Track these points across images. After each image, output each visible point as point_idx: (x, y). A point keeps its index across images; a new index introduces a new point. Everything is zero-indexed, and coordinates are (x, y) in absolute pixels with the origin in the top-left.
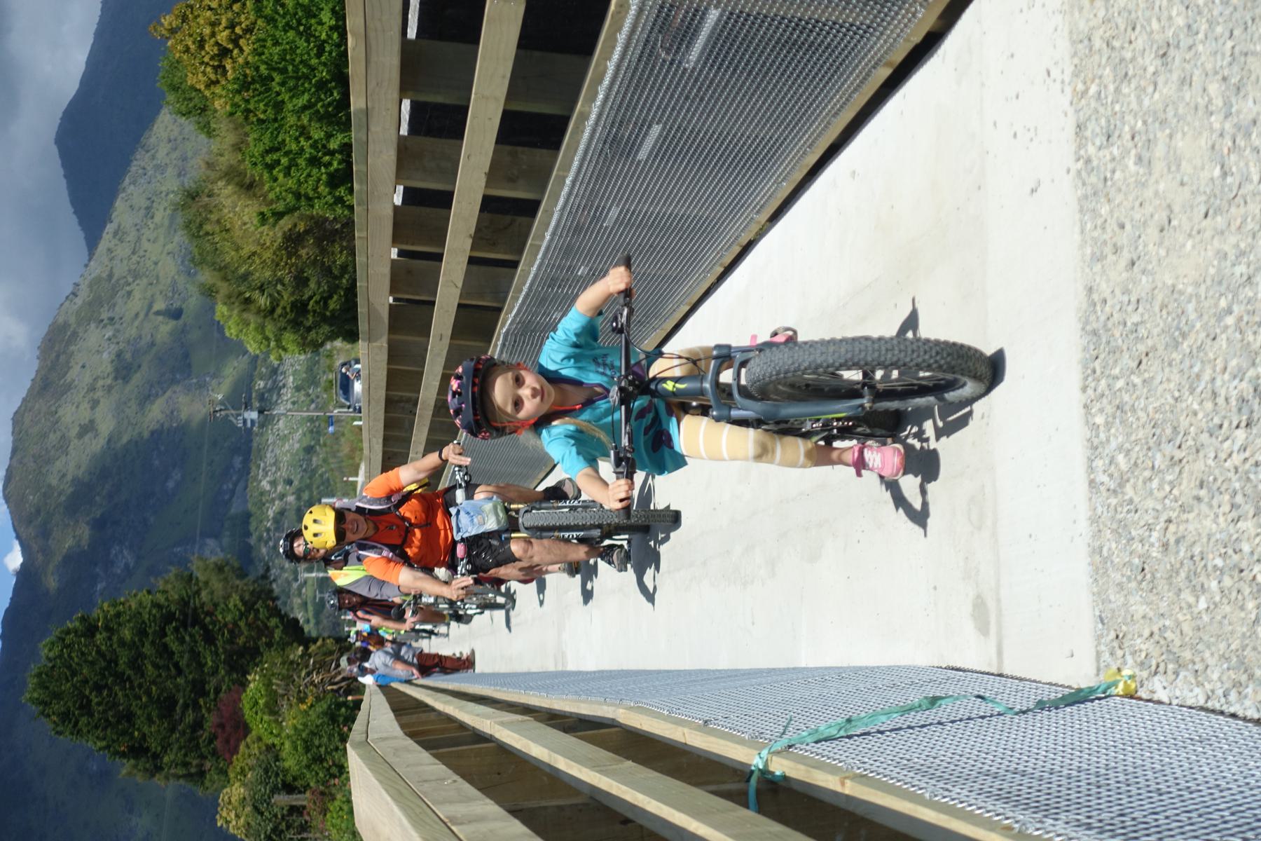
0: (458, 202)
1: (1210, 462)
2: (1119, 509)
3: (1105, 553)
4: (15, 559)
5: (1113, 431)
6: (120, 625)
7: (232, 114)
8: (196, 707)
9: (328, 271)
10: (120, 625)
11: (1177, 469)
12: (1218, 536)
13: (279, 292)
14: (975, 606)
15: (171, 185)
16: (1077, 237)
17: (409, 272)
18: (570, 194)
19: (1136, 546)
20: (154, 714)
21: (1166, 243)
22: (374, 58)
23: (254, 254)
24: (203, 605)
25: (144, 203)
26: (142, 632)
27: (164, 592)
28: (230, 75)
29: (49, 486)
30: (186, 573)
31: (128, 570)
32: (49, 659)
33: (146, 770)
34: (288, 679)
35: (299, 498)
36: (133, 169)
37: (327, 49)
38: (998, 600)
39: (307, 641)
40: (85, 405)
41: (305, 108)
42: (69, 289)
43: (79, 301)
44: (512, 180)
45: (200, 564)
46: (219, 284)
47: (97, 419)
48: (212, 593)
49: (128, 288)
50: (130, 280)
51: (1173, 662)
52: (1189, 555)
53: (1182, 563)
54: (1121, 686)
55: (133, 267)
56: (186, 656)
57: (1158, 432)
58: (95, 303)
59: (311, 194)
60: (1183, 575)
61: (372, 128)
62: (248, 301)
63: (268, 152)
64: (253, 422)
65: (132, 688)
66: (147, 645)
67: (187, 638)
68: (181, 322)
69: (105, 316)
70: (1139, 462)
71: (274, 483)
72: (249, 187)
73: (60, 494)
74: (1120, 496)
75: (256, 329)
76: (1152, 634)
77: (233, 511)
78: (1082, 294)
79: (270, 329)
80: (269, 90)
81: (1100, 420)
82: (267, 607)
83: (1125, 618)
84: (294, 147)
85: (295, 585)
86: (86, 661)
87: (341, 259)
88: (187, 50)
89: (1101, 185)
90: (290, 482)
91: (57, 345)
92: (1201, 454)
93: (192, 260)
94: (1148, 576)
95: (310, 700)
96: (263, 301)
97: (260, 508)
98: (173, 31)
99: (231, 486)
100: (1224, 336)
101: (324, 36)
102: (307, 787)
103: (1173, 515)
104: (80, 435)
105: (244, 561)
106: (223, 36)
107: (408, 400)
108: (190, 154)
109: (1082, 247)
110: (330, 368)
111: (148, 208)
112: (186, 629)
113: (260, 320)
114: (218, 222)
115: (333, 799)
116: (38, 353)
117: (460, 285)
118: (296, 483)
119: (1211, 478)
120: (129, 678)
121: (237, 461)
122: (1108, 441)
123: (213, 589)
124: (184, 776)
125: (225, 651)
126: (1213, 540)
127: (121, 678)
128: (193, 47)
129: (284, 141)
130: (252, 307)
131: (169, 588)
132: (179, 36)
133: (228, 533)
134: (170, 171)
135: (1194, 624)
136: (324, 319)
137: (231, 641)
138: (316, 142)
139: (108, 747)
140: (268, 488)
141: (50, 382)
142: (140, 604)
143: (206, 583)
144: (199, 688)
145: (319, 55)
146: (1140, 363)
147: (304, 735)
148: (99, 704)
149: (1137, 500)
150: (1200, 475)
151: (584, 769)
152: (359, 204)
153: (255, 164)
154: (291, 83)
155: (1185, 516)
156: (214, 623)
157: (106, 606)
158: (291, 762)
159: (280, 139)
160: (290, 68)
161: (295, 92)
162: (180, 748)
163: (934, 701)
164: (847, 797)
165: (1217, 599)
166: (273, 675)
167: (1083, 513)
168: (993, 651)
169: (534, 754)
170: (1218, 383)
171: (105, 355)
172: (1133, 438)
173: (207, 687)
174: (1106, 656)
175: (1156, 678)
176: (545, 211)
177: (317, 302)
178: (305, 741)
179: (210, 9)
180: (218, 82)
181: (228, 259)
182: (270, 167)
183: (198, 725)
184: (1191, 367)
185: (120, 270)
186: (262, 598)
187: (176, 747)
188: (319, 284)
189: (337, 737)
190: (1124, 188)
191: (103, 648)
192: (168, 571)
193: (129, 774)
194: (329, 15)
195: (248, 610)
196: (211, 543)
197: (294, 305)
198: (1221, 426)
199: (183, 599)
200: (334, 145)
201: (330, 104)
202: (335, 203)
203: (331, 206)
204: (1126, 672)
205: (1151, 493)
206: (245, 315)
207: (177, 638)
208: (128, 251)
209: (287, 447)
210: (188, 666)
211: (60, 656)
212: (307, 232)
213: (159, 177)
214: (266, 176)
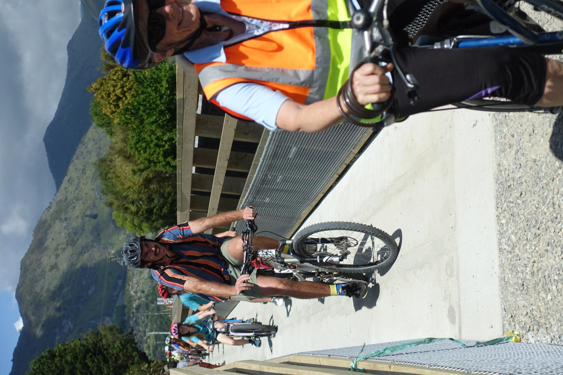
0: (222, 143)
1: (552, 234)
3: (506, 280)
4: (20, 325)
5: (509, 225)
6: (66, 354)
10: (66, 354)
11: (538, 239)
12: (556, 266)
13: (140, 205)
14: (449, 311)
15: (94, 159)
16: (494, 143)
17: (200, 179)
18: (271, 139)
19: (520, 275)
21: (532, 141)
23: (130, 187)
24: (103, 345)
25: (81, 167)
26: (76, 358)
27: (86, 340)
29: (36, 292)
30: (96, 331)
31: (70, 331)
35: (147, 299)
36: (77, 152)
37: (165, 97)
38: (460, 307)
39: (149, 362)
40: (53, 257)
41: (153, 123)
42: (47, 205)
43: (52, 210)
44: (246, 134)
45: (103, 327)
46: (114, 201)
47: (60, 262)
48: (107, 340)
49: (73, 205)
50: (75, 201)
51: (536, 325)
52: (543, 275)
53: (540, 280)
54: (514, 338)
55: (76, 196)
56: (95, 368)
57: (529, 223)
58: (59, 212)
60: (540, 285)
61: (186, 108)
62: (127, 208)
63: (137, 143)
66: (78, 364)
67: (96, 360)
68: (97, 220)
70: (521, 238)
71: (136, 292)
72: (128, 158)
74: (513, 254)
76: (527, 313)
77: (117, 305)
78: (495, 166)
79: (136, 222)
81: (503, 221)
82: (132, 347)
83: (515, 307)
86: (50, 370)
87: (168, 189)
88: (102, 97)
89: (504, 119)
90: (143, 292)
91: (41, 231)
92: (548, 231)
93: (103, 192)
94: (525, 287)
96: (133, 208)
97: (130, 303)
98: (97, 90)
99: (117, 293)
100: (557, 179)
101: (163, 92)
103: (536, 259)
104: (51, 270)
106: (118, 92)
108: (102, 146)
109: (495, 147)
111: (83, 170)
113: (132, 217)
114: (114, 173)
116: (33, 233)
117: (222, 184)
118: (146, 292)
119: (553, 241)
121: (120, 282)
122: (507, 230)
126: (554, 268)
128: (105, 96)
130: (129, 211)
131: (88, 337)
132: (99, 92)
133: (115, 314)
134: (94, 154)
135: (545, 307)
136: (160, 217)
137: (116, 362)
138: (158, 136)
140: (133, 294)
141: (39, 245)
142: (75, 344)
143: (105, 336)
146: (521, 194)
149: (520, 254)
150: (548, 240)
151: (275, 368)
152: (178, 145)
153: (132, 148)
154: (147, 111)
155: (542, 259)
156: (108, 354)
157: (60, 346)
160: (148, 105)
161: (149, 115)
163: (431, 340)
164: (392, 372)
165: (556, 294)
167: (497, 263)
170: (555, 199)
171: (63, 235)
172: (518, 227)
174: (507, 326)
175: (529, 333)
176: (260, 148)
177: (157, 210)
179: (113, 80)
181: (118, 190)
184: (543, 193)
185: (70, 197)
188: (159, 201)
190: (513, 119)
191: (58, 364)
192: (89, 330)
194: (165, 82)
195: (123, 349)
196: (107, 318)
198: (557, 218)
199: (94, 343)
200: (165, 138)
201: (165, 121)
202: (166, 165)
203: (164, 166)
204: (516, 333)
205: (526, 251)
206: (125, 215)
207: (91, 360)
208: (74, 188)
209: (142, 276)
211: (39, 368)
212: (154, 178)
213: (89, 156)
214: (137, 153)
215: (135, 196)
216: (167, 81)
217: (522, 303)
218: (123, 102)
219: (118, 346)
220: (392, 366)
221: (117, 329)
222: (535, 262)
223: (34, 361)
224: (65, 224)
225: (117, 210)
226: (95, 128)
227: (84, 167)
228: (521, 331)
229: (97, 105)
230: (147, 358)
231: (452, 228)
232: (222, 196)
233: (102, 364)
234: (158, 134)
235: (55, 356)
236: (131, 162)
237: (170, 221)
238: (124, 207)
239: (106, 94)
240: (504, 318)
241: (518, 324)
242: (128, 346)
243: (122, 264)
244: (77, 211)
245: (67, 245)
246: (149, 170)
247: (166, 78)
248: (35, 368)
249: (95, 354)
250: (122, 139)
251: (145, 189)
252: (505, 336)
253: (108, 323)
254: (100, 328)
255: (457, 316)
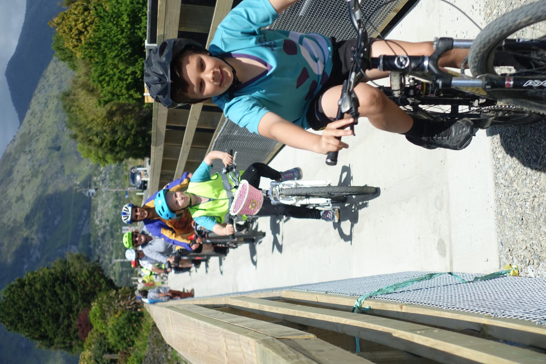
2: (510, 194)
5: (507, 160)
7: (84, 58)
8: (69, 318)
9: (125, 127)
10: (35, 282)
15: (56, 92)
17: (175, 114)
19: (519, 209)
20: (50, 321)
22: (169, 11)
24: (71, 274)
26: (45, 286)
27: (54, 268)
28: (83, 42)
31: (38, 260)
32: (4, 298)
33: (46, 345)
34: (110, 304)
37: (126, 30)
38: (450, 240)
39: (117, 289)
40: (19, 189)
42: (11, 138)
43: (16, 143)
46: (78, 133)
48: (75, 268)
49: (37, 138)
50: (38, 134)
53: (541, 215)
56: (64, 296)
58: (23, 144)
59: (119, 94)
60: (542, 220)
62: (91, 141)
63: (100, 76)
64: (93, 194)
65: (40, 310)
69: (27, 149)
71: (101, 221)
72: (92, 91)
73: (8, 227)
74: (510, 188)
75: (95, 154)
77: (83, 233)
79: (100, 154)
80: (100, 48)
83: (513, 242)
84: (111, 72)
85: (110, 265)
86: (21, 298)
88: (64, 32)
90: (108, 221)
94: (525, 222)
95: (119, 313)
96: (97, 140)
98: (58, 24)
101: (124, 26)
102: (118, 351)
104: (17, 201)
105: (88, 255)
106: (80, 26)
107: (170, 175)
108: (63, 80)
110: (126, 170)
111: (46, 103)
112: (64, 284)
113: (96, 149)
114: (77, 106)
115: (130, 355)
117: (198, 118)
118: (110, 221)
120: (39, 306)
121: (85, 212)
123: (75, 267)
124: (63, 348)
125: (81, 293)
127: (35, 305)
129: (107, 70)
130: (93, 143)
131: (56, 266)
132: (61, 26)
134: (55, 87)
136: (124, 149)
137: (84, 289)
138: (121, 70)
139: (30, 335)
143: (72, 264)
144: (70, 310)
145: (122, 34)
147: (117, 328)
148: (26, 317)
149: (518, 189)
151: (279, 308)
155: (543, 194)
156: (76, 281)
157: (29, 274)
158: (112, 340)
159: (105, 69)
162: (62, 336)
163: (431, 276)
164: (404, 313)
166: (103, 302)
167: (493, 197)
168: (448, 263)
169: (250, 307)
171: (27, 167)
173: (73, 309)
174: (504, 260)
175: (529, 267)
177: (121, 141)
178: (117, 331)
179: (75, 14)
180: (77, 46)
181: (82, 122)
182: (100, 82)
183: (69, 326)
185: (34, 130)
186: (97, 271)
187: (60, 336)
189: (131, 329)
191: (28, 293)
193: (39, 347)
196: (74, 247)
197: (111, 143)
200: (128, 72)
201: (127, 55)
202: (129, 98)
204: (514, 266)
206: (90, 147)
207: (60, 288)
209: (106, 205)
210: (65, 300)
211: (9, 296)
212: (117, 110)
214: (99, 86)
215: (99, 129)
216: (128, 15)
217: (521, 237)
218: (85, 37)
219: (85, 274)
220: (404, 307)
221: (84, 258)
222: (536, 197)
223: (3, 290)
224: (29, 157)
225: (81, 142)
226: (55, 62)
227: (45, 101)
228: (519, 265)
229: (59, 39)
230: (114, 284)
231: (442, 161)
232: (197, 130)
233: (71, 292)
234: (121, 68)
235: (25, 284)
236: (94, 95)
237: (134, 152)
238: (88, 139)
239: (68, 28)
240: (501, 252)
241: (516, 257)
242: (96, 273)
243: (87, 195)
244: (42, 144)
245: (32, 177)
246: (112, 102)
247: (127, 13)
248: (5, 296)
249: (63, 282)
250: (85, 73)
251: (109, 121)
252: (502, 269)
253: (74, 251)
254: (68, 257)
255: (448, 249)
